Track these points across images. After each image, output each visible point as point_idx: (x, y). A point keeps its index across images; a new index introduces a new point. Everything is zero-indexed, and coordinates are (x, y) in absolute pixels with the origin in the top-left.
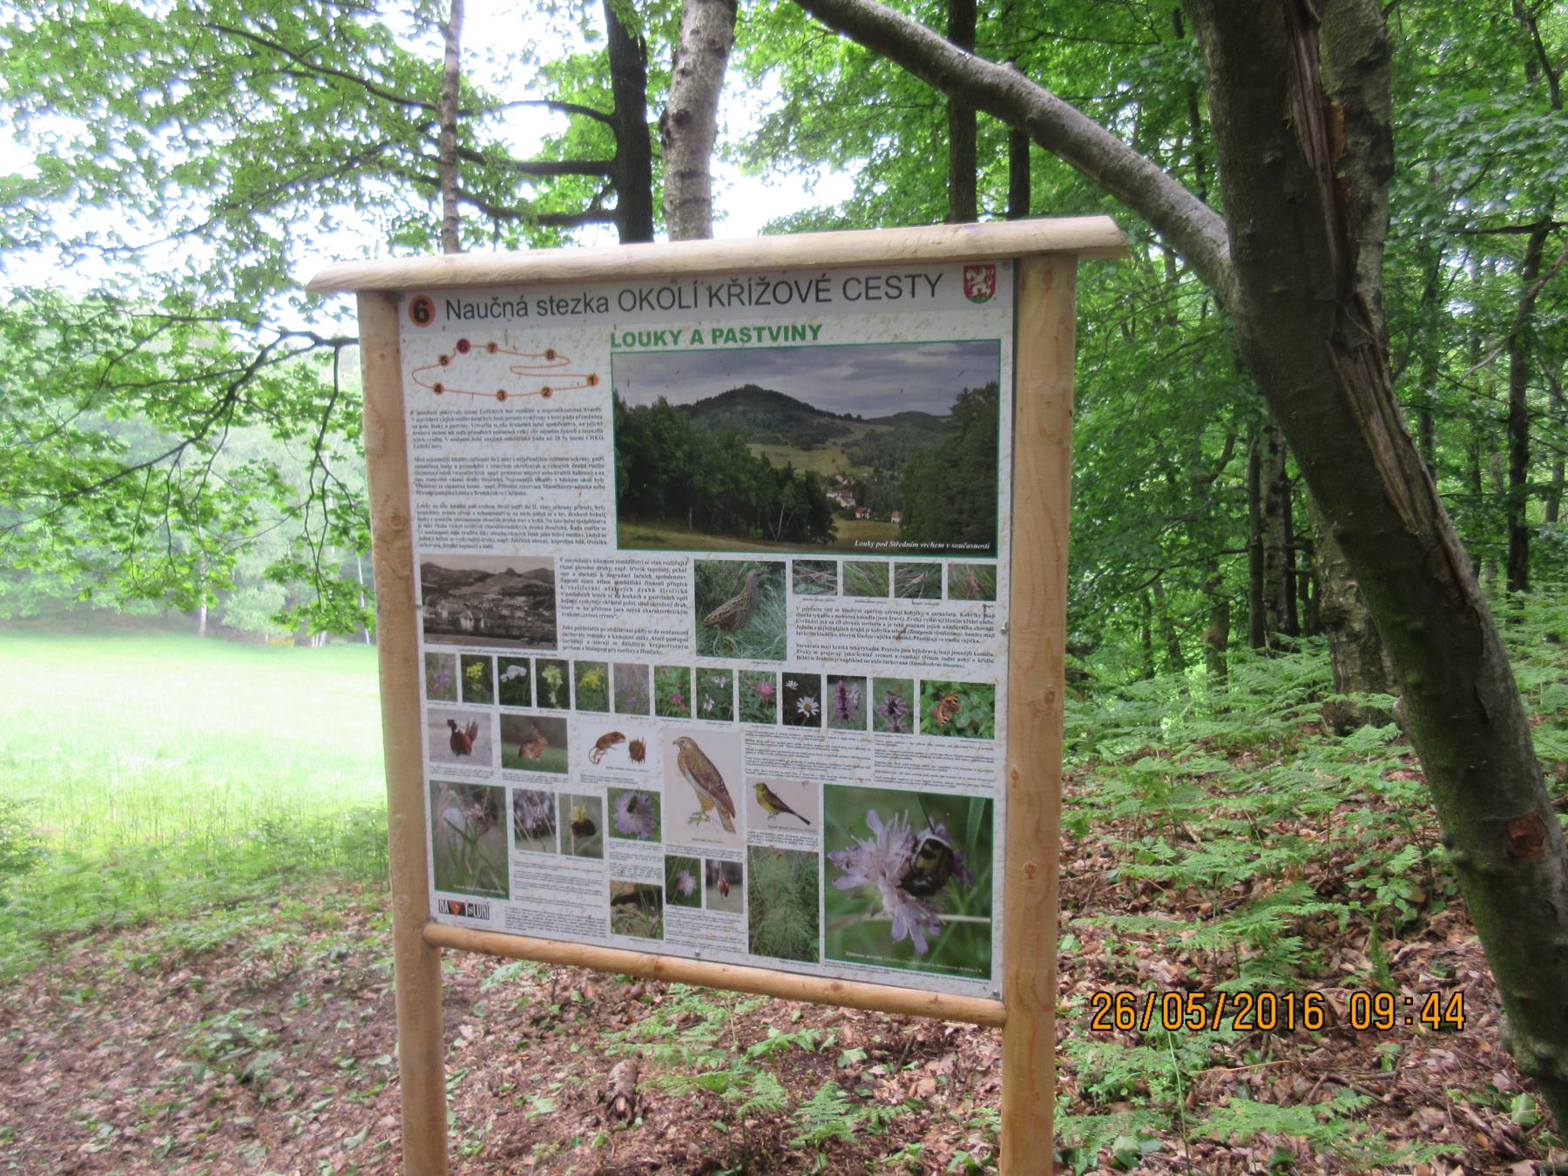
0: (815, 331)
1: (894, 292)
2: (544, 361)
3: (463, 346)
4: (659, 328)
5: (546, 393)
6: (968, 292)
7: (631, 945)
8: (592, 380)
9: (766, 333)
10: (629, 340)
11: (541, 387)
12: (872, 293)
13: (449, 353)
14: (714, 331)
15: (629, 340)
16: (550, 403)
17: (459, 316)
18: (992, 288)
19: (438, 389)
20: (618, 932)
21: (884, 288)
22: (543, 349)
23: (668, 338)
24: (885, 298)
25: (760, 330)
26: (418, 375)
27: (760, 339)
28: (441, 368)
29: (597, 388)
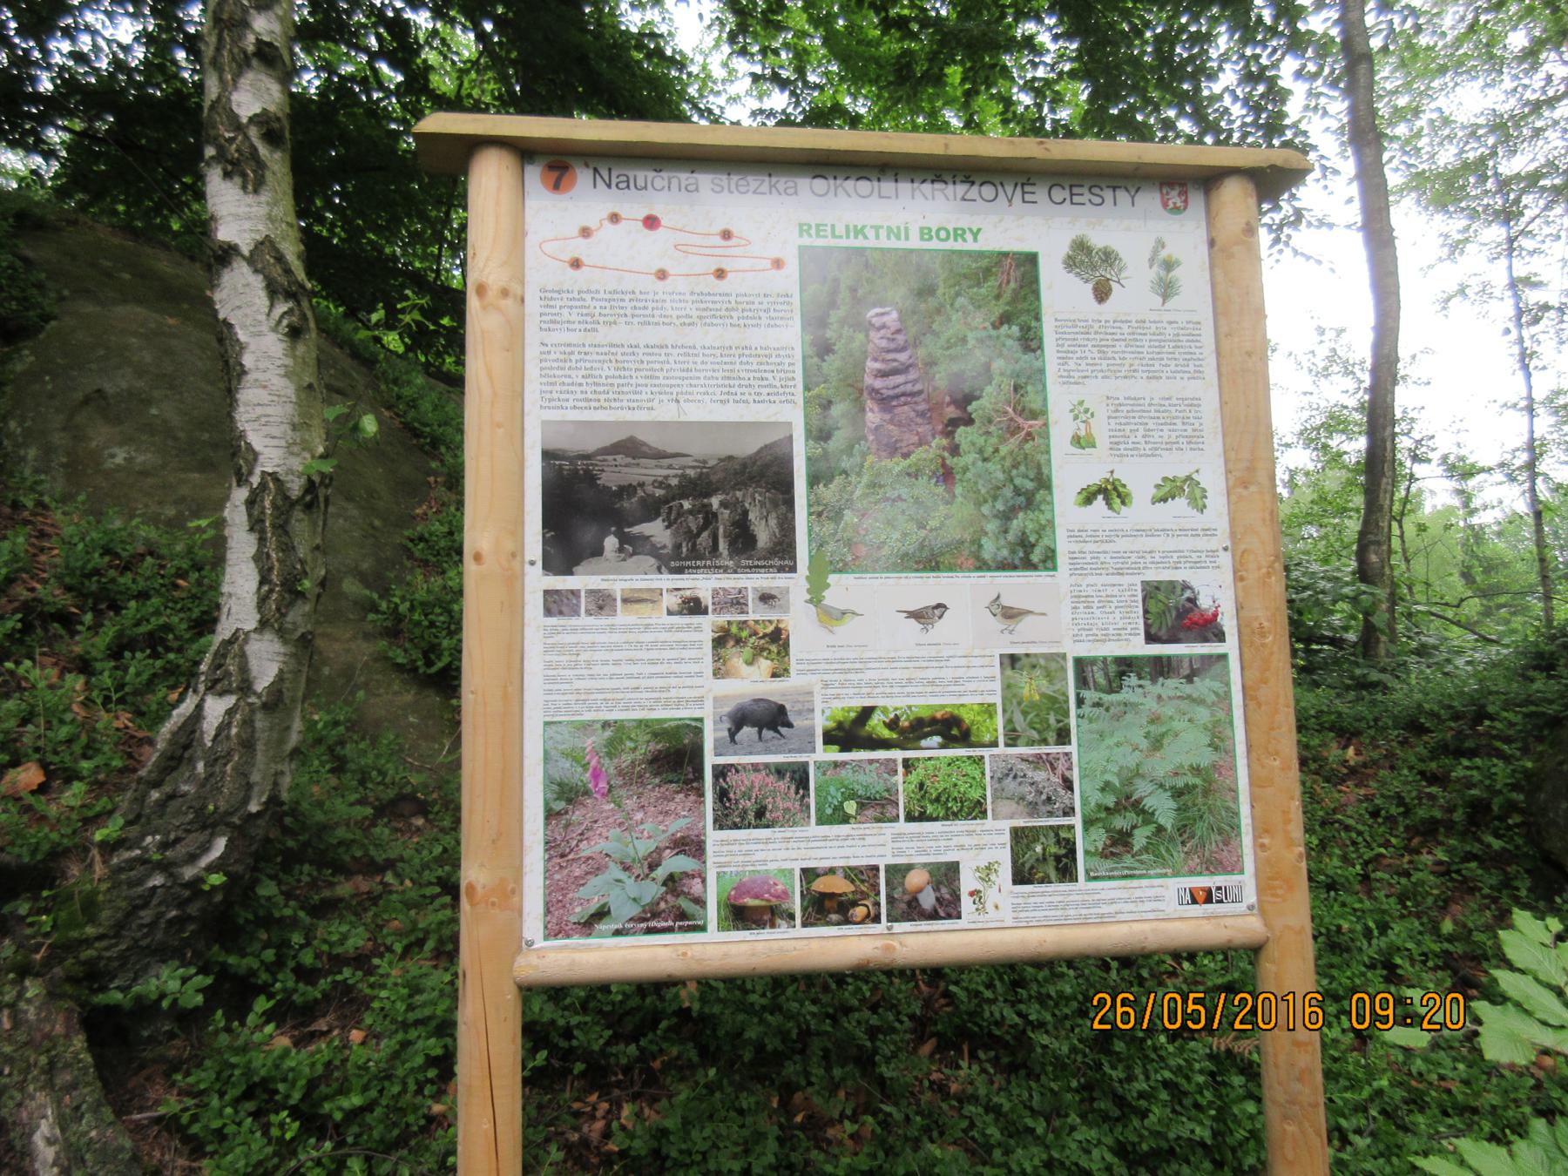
0: (975, 235)
1: (1097, 200)
2: (718, 241)
3: (615, 218)
4: (963, 224)
5: (720, 274)
6: (1165, 205)
7: (577, 956)
8: (778, 264)
9: (883, 233)
10: (943, 234)
11: (713, 268)
12: (1076, 199)
13: (593, 225)
14: (922, 229)
15: (943, 234)
16: (722, 286)
17: (609, 186)
18: (1186, 201)
19: (576, 264)
20: (721, 828)
21: (1088, 196)
22: (719, 227)
23: (871, 233)
24: (979, 200)
25: (877, 228)
26: (548, 247)
27: (877, 237)
28: (581, 241)
29: (783, 272)
